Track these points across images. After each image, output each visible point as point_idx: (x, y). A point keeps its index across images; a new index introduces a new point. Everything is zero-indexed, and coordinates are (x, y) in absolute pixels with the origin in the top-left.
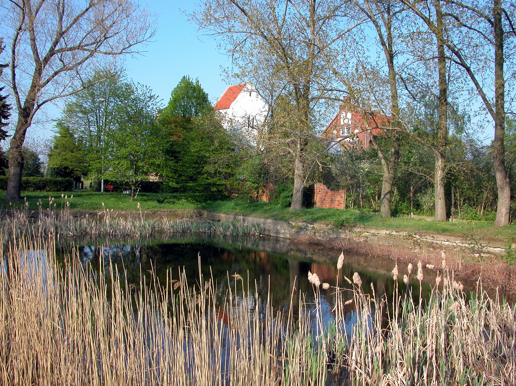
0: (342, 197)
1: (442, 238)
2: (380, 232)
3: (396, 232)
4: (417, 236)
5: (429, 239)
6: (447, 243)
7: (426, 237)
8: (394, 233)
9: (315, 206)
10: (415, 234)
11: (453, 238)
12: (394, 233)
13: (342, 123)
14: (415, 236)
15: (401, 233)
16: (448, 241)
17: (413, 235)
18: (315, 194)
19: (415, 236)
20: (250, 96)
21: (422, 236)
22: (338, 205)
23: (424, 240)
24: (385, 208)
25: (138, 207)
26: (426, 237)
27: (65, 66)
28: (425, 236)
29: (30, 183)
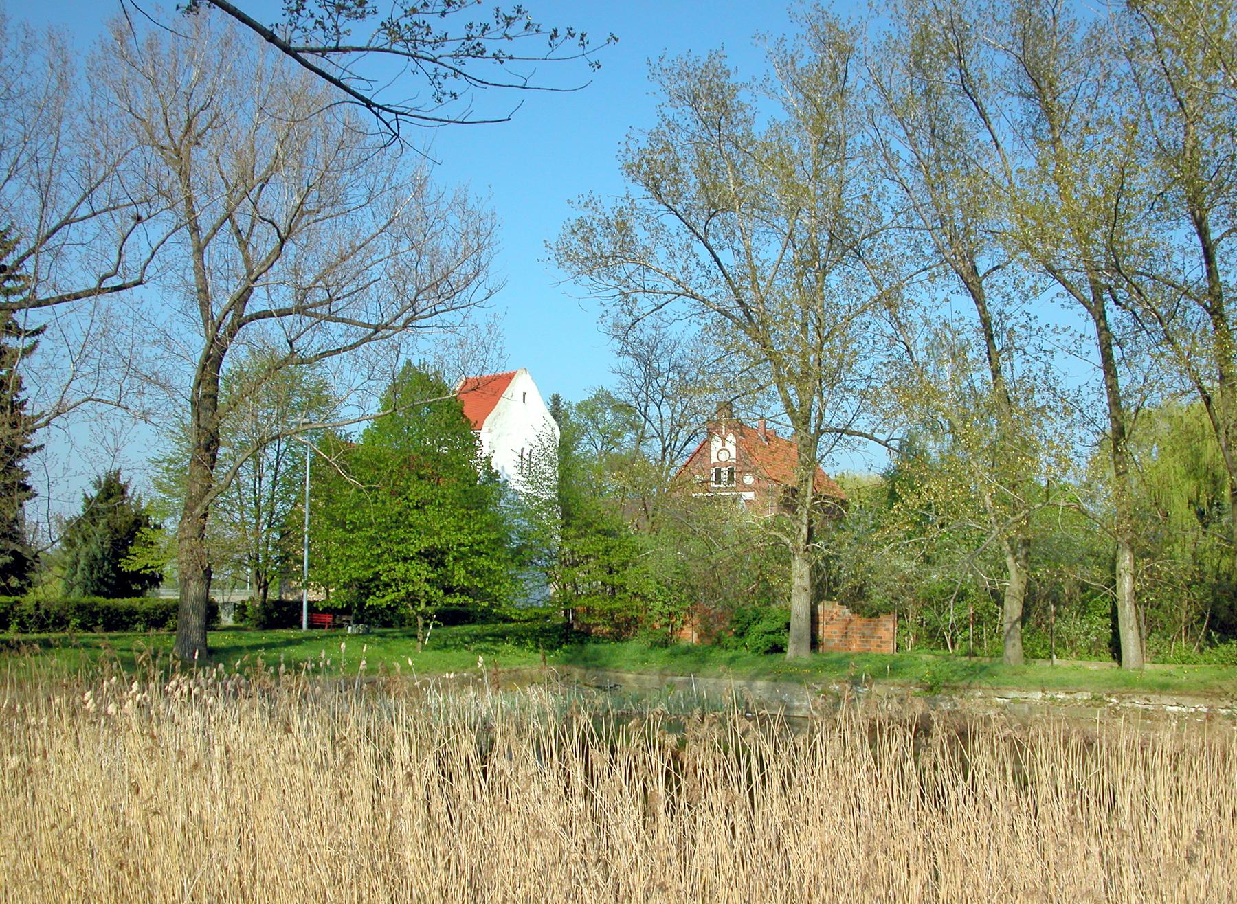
0: (887, 630)
1: (1165, 700)
2: (1030, 696)
3: (1066, 693)
4: (1113, 700)
5: (1139, 703)
6: (1175, 709)
7: (1133, 700)
8: (1061, 696)
9: (821, 650)
10: (1109, 696)
11: (1189, 699)
12: (1061, 696)
13: (714, 460)
14: (1108, 699)
15: (1079, 696)
16: (1178, 705)
17: (1105, 698)
18: (821, 626)
19: (1108, 699)
20: (525, 393)
21: (1123, 698)
22: (878, 646)
23: (1129, 705)
24: (1013, 649)
25: (480, 665)
26: (1133, 700)
27: (292, 353)
28: (1129, 698)
29: (137, 613)
